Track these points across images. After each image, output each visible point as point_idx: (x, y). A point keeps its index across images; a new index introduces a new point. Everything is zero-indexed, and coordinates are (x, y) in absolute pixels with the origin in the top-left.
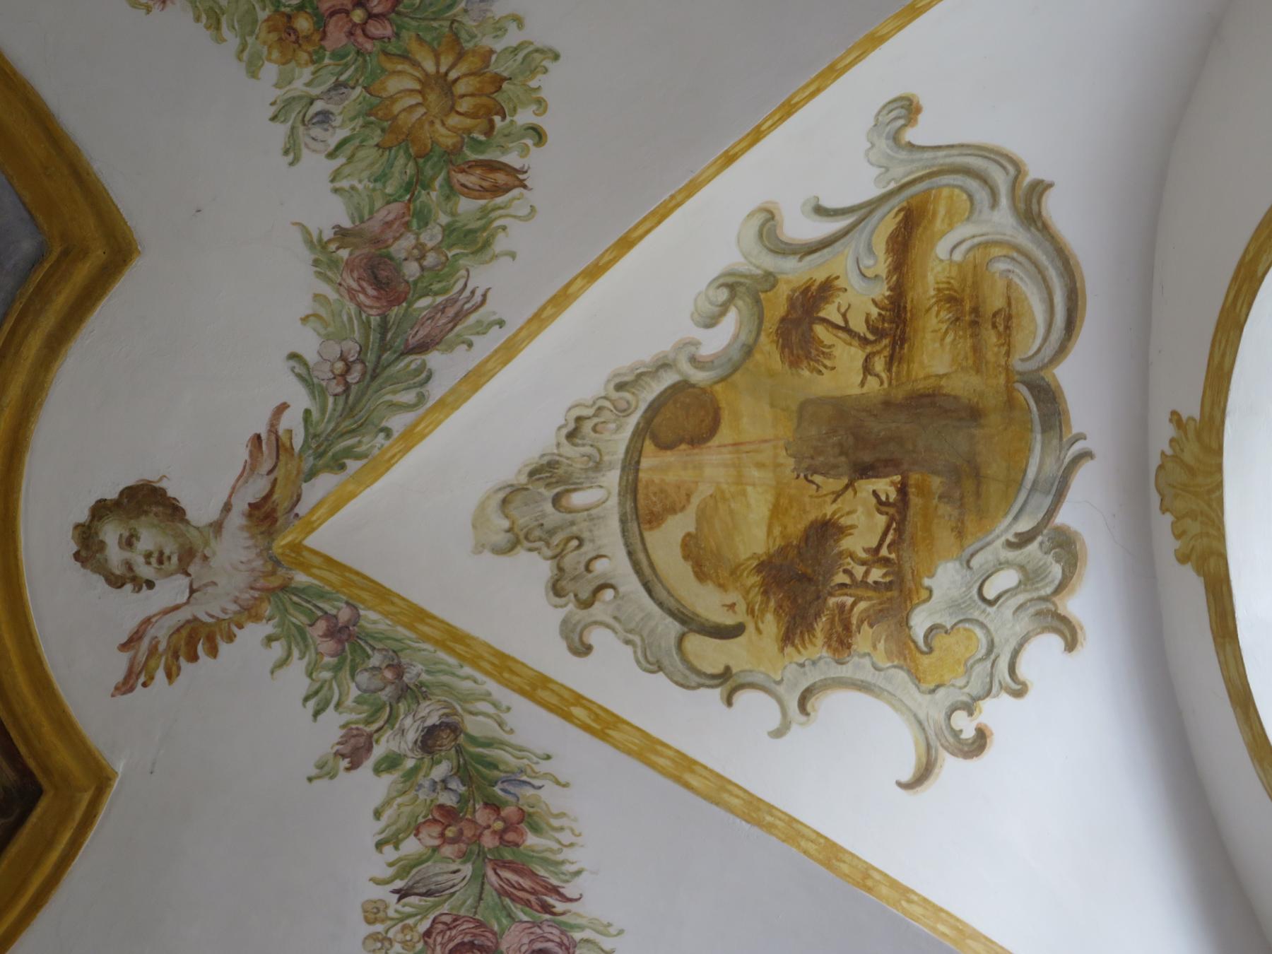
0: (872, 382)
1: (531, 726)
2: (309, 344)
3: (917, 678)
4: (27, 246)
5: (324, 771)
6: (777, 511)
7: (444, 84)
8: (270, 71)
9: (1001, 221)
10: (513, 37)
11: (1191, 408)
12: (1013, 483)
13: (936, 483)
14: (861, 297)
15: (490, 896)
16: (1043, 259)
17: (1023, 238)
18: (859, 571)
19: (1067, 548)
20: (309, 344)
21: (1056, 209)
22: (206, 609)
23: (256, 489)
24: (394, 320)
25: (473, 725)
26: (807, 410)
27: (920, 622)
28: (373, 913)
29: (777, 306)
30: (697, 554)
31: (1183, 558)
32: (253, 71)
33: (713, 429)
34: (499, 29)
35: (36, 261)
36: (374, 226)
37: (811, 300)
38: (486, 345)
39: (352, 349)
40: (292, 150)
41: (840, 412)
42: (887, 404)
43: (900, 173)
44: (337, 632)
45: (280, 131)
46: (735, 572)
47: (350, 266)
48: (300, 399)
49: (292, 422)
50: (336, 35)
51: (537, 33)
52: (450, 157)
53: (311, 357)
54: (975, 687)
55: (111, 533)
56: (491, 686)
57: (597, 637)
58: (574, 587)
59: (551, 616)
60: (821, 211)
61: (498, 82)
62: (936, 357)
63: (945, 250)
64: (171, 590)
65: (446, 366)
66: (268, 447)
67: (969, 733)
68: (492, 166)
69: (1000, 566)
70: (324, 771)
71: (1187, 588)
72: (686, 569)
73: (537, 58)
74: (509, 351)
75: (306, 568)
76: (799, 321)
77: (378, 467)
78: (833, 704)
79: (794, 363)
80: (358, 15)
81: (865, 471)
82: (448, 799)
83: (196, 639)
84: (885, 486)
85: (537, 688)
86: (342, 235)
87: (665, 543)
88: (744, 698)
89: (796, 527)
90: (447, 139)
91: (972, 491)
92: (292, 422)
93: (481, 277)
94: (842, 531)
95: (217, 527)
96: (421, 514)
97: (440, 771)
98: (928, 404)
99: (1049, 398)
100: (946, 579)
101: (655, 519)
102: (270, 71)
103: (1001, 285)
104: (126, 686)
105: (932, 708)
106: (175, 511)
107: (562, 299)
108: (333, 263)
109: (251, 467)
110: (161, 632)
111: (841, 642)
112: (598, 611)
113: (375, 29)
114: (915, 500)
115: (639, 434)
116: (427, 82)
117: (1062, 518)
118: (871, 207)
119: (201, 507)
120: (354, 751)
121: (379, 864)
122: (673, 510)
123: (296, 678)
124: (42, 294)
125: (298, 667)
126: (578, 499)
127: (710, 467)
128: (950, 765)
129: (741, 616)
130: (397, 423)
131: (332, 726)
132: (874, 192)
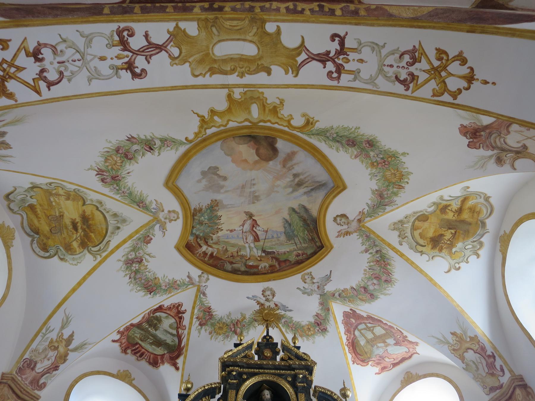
0: (454, 218)
1: (391, 253)
2: (369, 202)
3: (451, 257)
4: (332, 185)
5: (362, 252)
6: (435, 232)
7: (395, 174)
8: (369, 169)
9: (482, 200)
10: (406, 170)
11: (508, 232)
12: (474, 234)
13: (461, 232)
14: (455, 206)
15: (381, 272)
16: (488, 206)
17: (485, 203)
18: (446, 241)
19: (481, 244)
20: (369, 202)
21: (491, 200)
22: (349, 230)
23: (359, 217)
24: (381, 202)
25: (383, 251)
26: (442, 220)
27: (454, 250)
28: (365, 270)
29: (441, 206)
30: (421, 236)
31: (500, 251)
32: (367, 169)
33: (427, 220)
34: (404, 169)
35: (333, 187)
36: (381, 190)
37: (446, 207)
38: (394, 207)
39: (375, 204)
40: (371, 179)
41: (448, 221)
42: (456, 221)
43: (465, 193)
44: (367, 236)
45: (370, 177)
46: (426, 238)
47: (377, 194)
48: (367, 208)
49: (365, 211)
50: (380, 166)
51: (410, 170)
52: (394, 183)
53: (369, 203)
54: (460, 261)
55: (338, 219)
56: (387, 247)
57: (403, 243)
58: (402, 236)
59: (398, 239)
60: (450, 196)
61: (403, 175)
62: (465, 216)
63: (470, 203)
64: (345, 227)
65: (388, 208)
66: (362, 213)
67: (457, 267)
68: (400, 185)
69: (469, 244)
70: (362, 252)
71: (499, 256)
72: (419, 237)
73: (409, 173)
74: (398, 208)
75: (364, 228)
76: (444, 209)
77: (376, 218)
78: (436, 259)
79: (442, 214)
80: (383, 164)
81: (450, 229)
82: (378, 259)
83: (347, 233)
84: (453, 231)
85: (393, 249)
86: (376, 190)
87: (417, 233)
88: (424, 255)
89: (437, 234)
90: (394, 181)
91: (467, 234)
92: (365, 211)
93: (395, 198)
94: (444, 236)
95: (353, 221)
96: (382, 225)
97: (377, 256)
98: (463, 222)
99: (484, 224)
100: (460, 245)
101: (416, 230)
102: (369, 169)
103: (479, 208)
104: (337, 237)
105: (452, 262)
106: (348, 218)
107: (407, 203)
108: (375, 193)
109: (359, 215)
110: (343, 231)
111: (441, 250)
112: (405, 240)
113: (386, 166)
114: (457, 234)
115: (416, 219)
116: (392, 174)
117: (481, 240)
118: (458, 197)
119: (351, 217)
120: (366, 251)
121: (367, 265)
122: (419, 229)
123: (360, 240)
124: (333, 191)
125: (361, 239)
126: (405, 225)
127: (426, 224)
128: (453, 271)
129: (426, 244)
130: (380, 214)
131: (364, 247)
132: (459, 195)
